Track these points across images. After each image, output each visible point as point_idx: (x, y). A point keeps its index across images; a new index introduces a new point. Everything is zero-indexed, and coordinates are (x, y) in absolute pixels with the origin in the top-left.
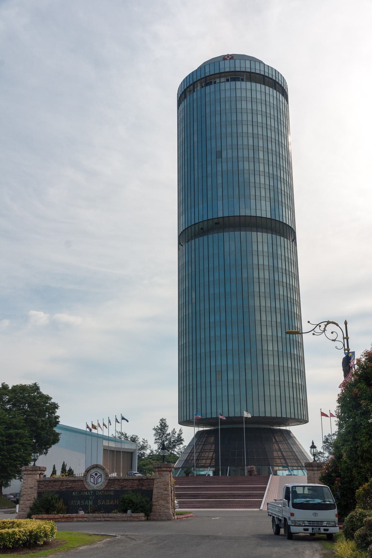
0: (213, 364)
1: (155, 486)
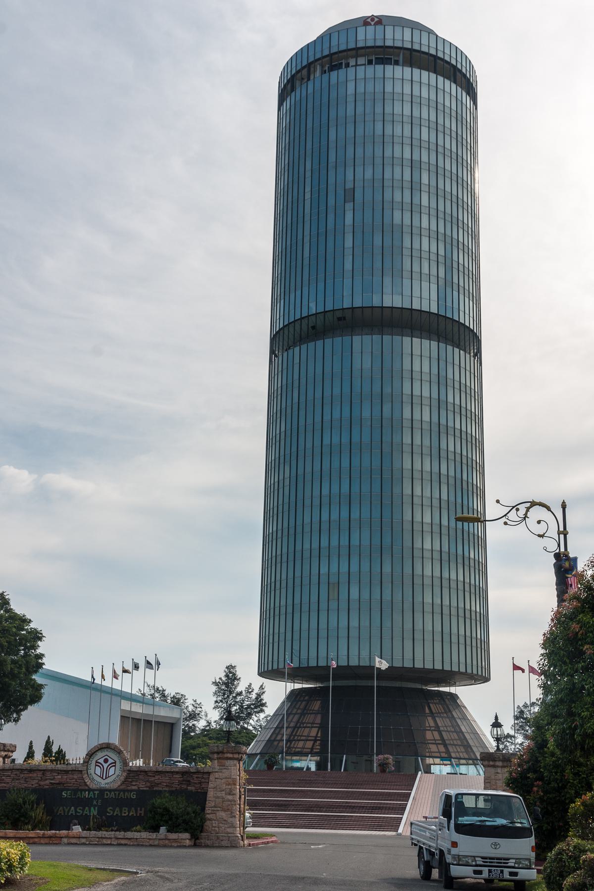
0: (324, 570)
1: (211, 785)
